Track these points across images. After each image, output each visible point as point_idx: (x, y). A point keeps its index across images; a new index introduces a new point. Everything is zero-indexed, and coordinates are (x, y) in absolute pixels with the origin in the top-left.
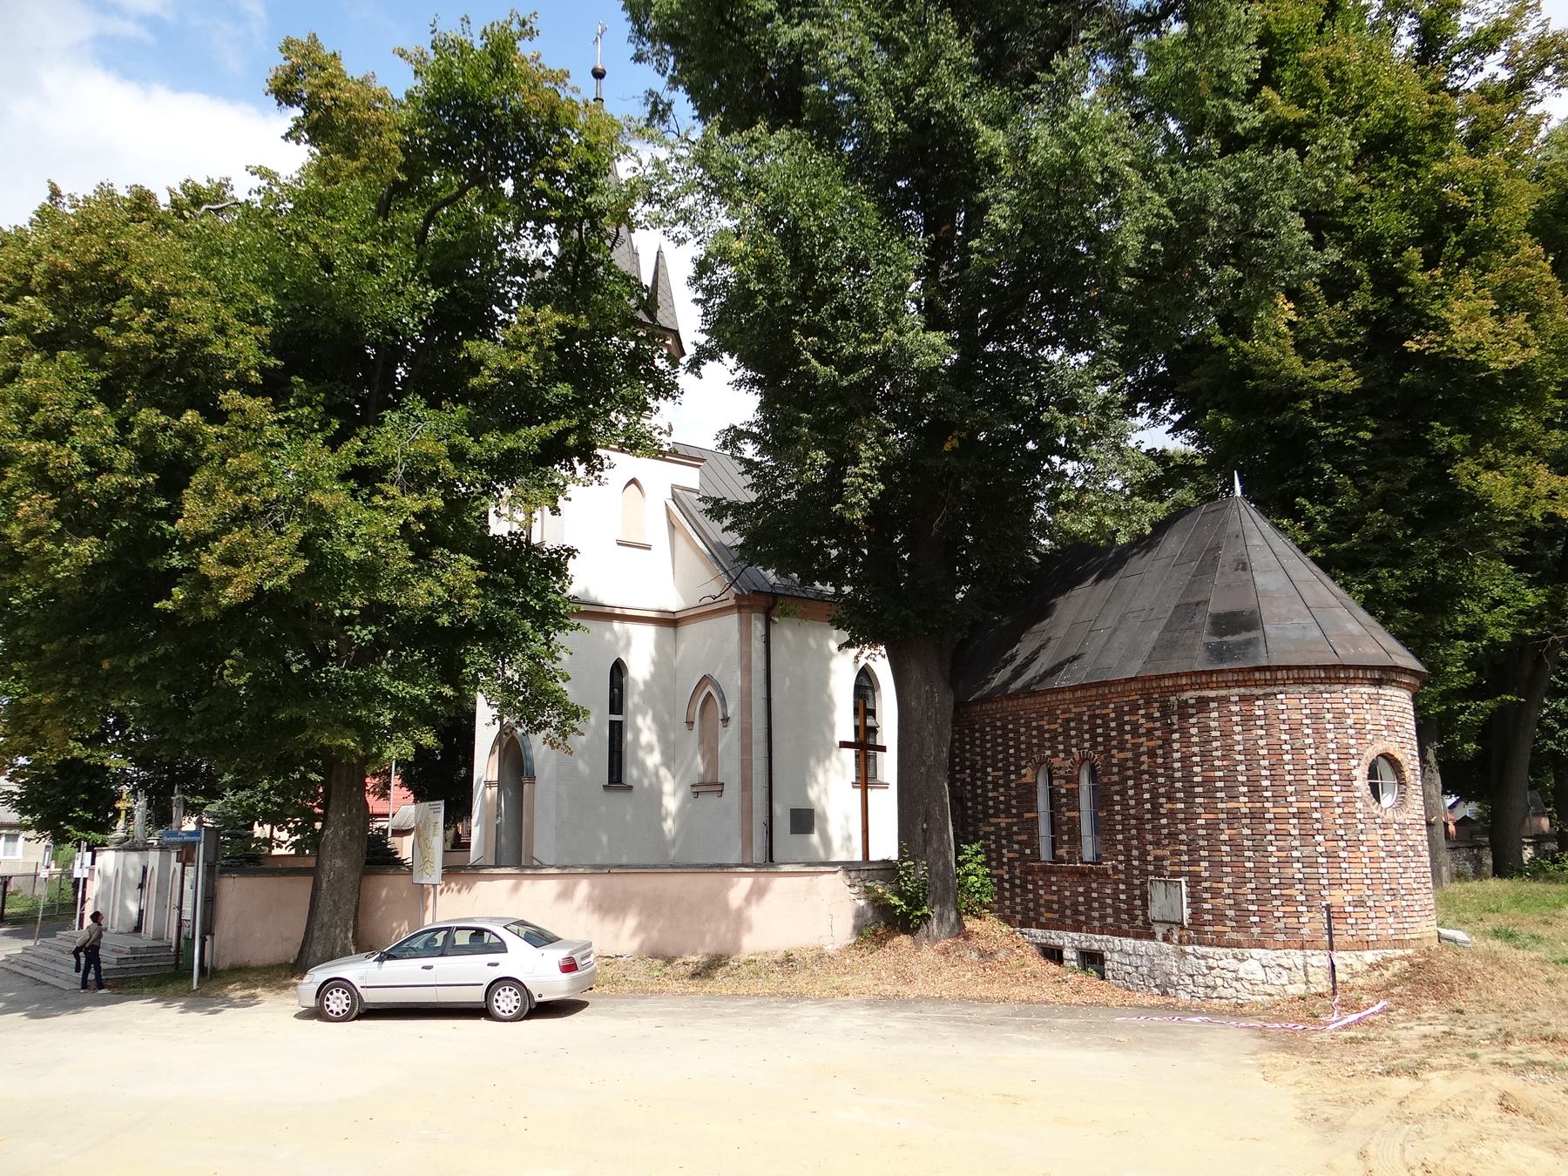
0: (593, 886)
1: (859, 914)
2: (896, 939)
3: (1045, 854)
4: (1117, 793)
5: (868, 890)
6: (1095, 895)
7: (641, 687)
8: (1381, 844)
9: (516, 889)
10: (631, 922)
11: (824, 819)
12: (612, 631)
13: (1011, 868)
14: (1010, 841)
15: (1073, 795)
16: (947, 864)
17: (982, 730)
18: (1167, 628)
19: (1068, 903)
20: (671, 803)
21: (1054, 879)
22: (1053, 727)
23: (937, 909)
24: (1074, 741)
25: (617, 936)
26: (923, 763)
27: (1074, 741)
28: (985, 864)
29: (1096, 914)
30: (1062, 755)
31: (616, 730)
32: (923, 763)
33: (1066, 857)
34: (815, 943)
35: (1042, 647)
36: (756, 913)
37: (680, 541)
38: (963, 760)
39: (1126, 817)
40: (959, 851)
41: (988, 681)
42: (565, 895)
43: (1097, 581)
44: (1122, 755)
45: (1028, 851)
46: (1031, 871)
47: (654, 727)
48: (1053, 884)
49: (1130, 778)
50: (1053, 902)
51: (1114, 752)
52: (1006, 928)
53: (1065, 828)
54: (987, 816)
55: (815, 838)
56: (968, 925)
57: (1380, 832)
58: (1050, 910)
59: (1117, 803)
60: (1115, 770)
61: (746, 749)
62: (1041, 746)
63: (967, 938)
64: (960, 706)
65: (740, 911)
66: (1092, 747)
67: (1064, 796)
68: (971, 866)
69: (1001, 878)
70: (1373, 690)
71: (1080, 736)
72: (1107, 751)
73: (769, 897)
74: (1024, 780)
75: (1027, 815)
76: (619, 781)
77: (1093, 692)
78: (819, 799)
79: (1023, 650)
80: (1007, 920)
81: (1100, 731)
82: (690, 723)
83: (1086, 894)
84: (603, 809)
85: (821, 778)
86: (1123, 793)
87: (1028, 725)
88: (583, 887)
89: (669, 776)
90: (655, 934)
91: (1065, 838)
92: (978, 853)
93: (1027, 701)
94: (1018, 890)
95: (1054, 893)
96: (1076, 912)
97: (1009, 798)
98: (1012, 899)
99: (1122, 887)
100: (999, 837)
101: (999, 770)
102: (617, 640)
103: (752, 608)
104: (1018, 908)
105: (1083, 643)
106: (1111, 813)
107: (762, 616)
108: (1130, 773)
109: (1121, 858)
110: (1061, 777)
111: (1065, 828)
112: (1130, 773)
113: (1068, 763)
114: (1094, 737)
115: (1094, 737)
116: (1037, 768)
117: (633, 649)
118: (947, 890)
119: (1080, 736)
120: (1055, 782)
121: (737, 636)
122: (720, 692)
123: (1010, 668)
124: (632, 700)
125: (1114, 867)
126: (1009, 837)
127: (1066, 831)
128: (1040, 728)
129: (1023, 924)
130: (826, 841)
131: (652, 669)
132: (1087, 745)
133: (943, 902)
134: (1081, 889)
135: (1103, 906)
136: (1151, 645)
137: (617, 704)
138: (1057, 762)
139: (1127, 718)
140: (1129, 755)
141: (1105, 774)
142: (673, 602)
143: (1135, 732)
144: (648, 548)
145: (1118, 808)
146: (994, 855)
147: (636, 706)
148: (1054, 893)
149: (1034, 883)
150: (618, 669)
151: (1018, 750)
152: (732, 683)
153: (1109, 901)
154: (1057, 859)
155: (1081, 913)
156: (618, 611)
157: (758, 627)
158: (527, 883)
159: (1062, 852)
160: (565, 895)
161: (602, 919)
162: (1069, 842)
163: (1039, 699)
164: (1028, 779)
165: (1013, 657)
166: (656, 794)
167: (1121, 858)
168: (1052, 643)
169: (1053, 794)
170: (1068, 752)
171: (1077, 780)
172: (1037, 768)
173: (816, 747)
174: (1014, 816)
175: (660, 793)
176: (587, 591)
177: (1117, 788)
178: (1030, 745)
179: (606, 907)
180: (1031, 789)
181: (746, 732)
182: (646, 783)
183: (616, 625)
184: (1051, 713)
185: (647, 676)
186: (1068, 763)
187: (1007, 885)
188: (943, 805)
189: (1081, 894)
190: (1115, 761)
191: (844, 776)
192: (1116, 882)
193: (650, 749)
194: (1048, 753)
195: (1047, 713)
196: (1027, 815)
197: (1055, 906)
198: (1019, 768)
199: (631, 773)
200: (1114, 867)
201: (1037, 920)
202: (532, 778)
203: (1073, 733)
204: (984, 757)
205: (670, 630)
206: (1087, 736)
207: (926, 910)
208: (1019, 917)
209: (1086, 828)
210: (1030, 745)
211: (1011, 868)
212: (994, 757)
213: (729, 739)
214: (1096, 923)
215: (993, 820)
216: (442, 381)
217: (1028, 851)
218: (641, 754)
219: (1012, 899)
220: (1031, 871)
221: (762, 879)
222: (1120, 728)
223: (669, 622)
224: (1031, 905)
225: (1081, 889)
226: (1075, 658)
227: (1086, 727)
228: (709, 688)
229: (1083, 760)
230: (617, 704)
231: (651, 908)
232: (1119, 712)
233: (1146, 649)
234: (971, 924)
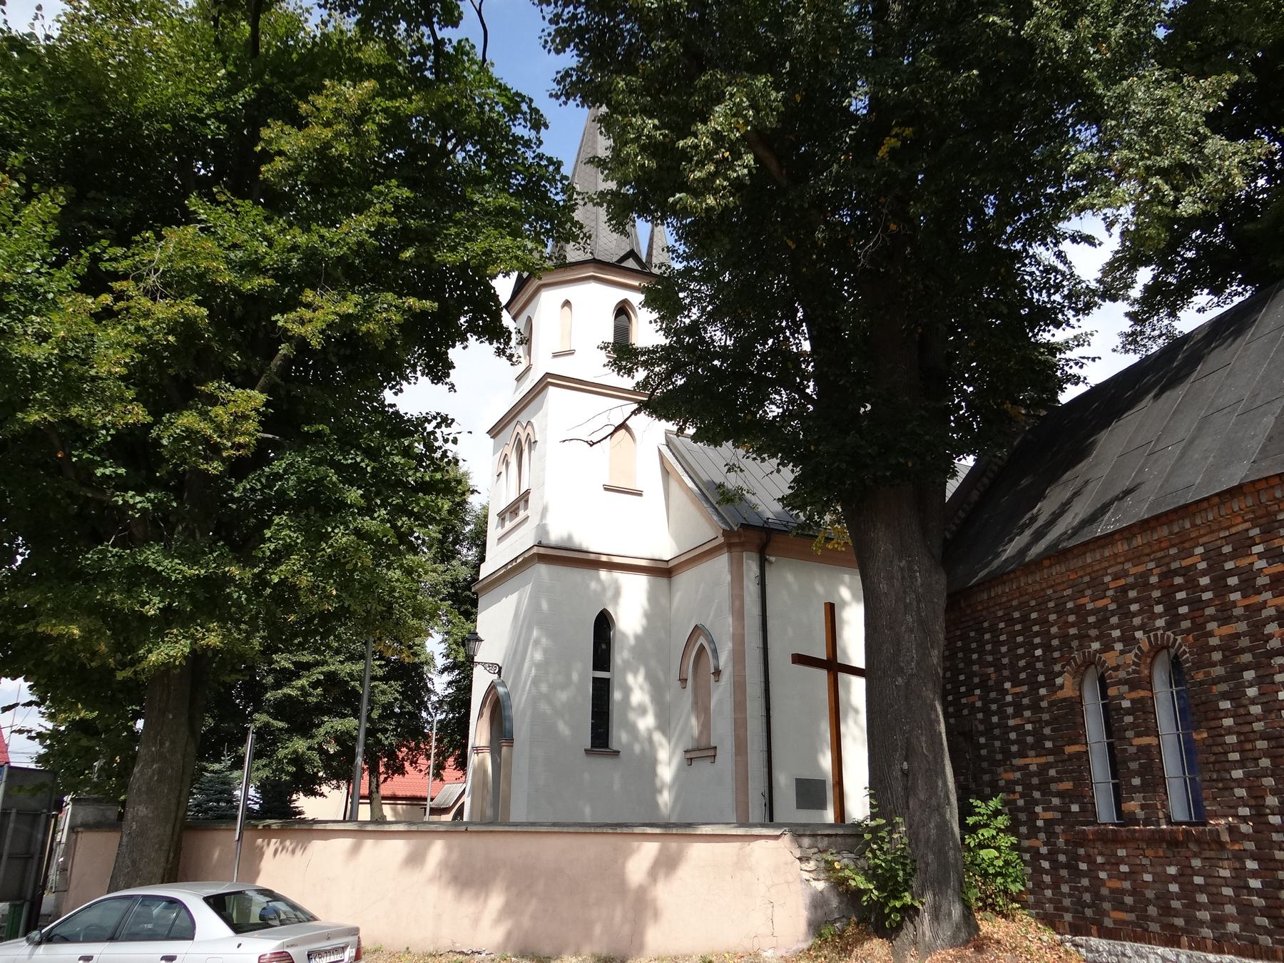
0: (450, 849)
1: (817, 903)
2: (867, 946)
3: (1105, 811)
4: (1224, 696)
5: (829, 866)
6: (1198, 880)
7: (632, 641)
9: (355, 849)
10: (496, 901)
12: (599, 580)
13: (1051, 835)
14: (1046, 792)
15: (1144, 709)
16: (944, 826)
17: (994, 630)
18: (1205, 949)
19: (1150, 894)
20: (666, 773)
21: (1122, 852)
22: (1100, 604)
23: (928, 898)
24: (1137, 621)
25: (476, 921)
26: (900, 671)
27: (1137, 621)
28: (1011, 830)
29: (1204, 915)
30: (1119, 646)
31: (602, 692)
32: (900, 671)
33: (1140, 814)
34: (748, 945)
35: (1076, 494)
36: (666, 893)
37: (674, 486)
38: (970, 676)
39: (1247, 738)
40: (965, 810)
41: (998, 555)
42: (415, 859)
43: (1156, 397)
44: (1226, 630)
45: (1075, 808)
46: (1082, 840)
47: (646, 687)
48: (1121, 861)
49: (1247, 667)
50: (1123, 892)
51: (1212, 626)
52: (1048, 936)
53: (1134, 765)
54: (1008, 755)
56: (985, 928)
58: (1120, 906)
59: (1227, 713)
60: (1217, 656)
61: (740, 705)
62: (1084, 638)
63: (979, 949)
64: (957, 600)
65: (642, 892)
66: (1169, 626)
67: (1129, 712)
68: (987, 833)
69: (1036, 855)
71: (1147, 610)
72: (1199, 628)
73: (685, 872)
74: (1060, 694)
75: (1070, 749)
76: (606, 745)
77: (1164, 531)
79: (1045, 509)
80: (1050, 921)
81: (1181, 595)
82: (683, 681)
83: (1184, 876)
84: (586, 776)
86: (1236, 695)
87: (1060, 610)
88: (437, 850)
89: (664, 741)
90: (526, 922)
91: (1136, 781)
92: (997, 813)
93: (1056, 569)
94: (1064, 873)
95: (1125, 877)
96: (1167, 911)
97: (1038, 723)
98: (1055, 886)
99: (1251, 865)
100: (1028, 788)
101: (1022, 683)
102: (604, 589)
103: (743, 546)
104: (1067, 902)
105: (1141, 471)
106: (1217, 734)
107: (755, 556)
108: (1247, 658)
109: (1244, 811)
110: (1121, 682)
111: (1134, 765)
112: (1247, 658)
113: (1131, 657)
114: (1171, 607)
115: (1171, 607)
116: (1079, 675)
117: (623, 601)
118: (944, 866)
119: (1147, 610)
120: (1112, 692)
121: (729, 578)
122: (712, 642)
123: (1028, 533)
124: (620, 656)
125: (1232, 829)
126: (1044, 786)
127: (1131, 769)
128: (1080, 611)
129: (1076, 930)
131: (644, 622)
132: (1160, 623)
133: (939, 885)
134: (1172, 870)
135: (1216, 901)
136: (1262, 438)
137: (602, 658)
138: (1111, 659)
139: (1229, 565)
140: (1242, 627)
141: (1198, 666)
142: (666, 550)
143: (1248, 586)
144: (639, 494)
145: (1228, 722)
146: (1023, 817)
147: (626, 662)
148: (1125, 877)
149: (1090, 859)
150: (604, 623)
151: (1047, 648)
152: (723, 630)
153: (1227, 891)
154: (1125, 818)
155: (1176, 913)
156: (604, 558)
157: (751, 567)
158: (369, 843)
159: (1133, 806)
160: (415, 859)
161: (460, 894)
162: (1144, 788)
163: (1075, 563)
164: (1068, 692)
165: (1033, 519)
166: (650, 763)
167: (1244, 811)
168: (1089, 487)
169: (1110, 712)
170: (1128, 640)
171: (1149, 684)
172: (1079, 675)
174: (1050, 752)
175: (654, 762)
176: (570, 538)
177: (1223, 687)
178: (1065, 639)
179: (466, 879)
180: (1074, 707)
181: (739, 687)
182: (637, 748)
183: (603, 574)
184: (1098, 587)
185: (639, 630)
186: (1131, 657)
187: (1046, 865)
188: (936, 736)
189: (1174, 879)
190: (1214, 641)
192: (1239, 857)
193: (642, 711)
194: (1096, 646)
195: (1089, 585)
196: (1070, 749)
197: (1129, 900)
198: (1051, 677)
199: (619, 737)
200: (1232, 829)
201: (1099, 924)
202: (511, 741)
203: (1134, 607)
204: (999, 667)
205: (663, 581)
206: (1159, 609)
207: (908, 898)
208: (1068, 917)
209: (1171, 763)
210: (1065, 639)
211: (1051, 835)
212: (1013, 665)
213: (721, 694)
214: (1207, 932)
215: (1018, 762)
216: (240, 171)
217: (1075, 808)
218: (632, 716)
219: (1055, 886)
220: (1082, 840)
221: (673, 845)
222: (1219, 586)
223: (661, 571)
224: (1087, 897)
225: (1172, 870)
226: (1127, 493)
227: (1156, 594)
228: (702, 640)
229: (1157, 649)
230: (602, 658)
231: (522, 884)
232: (1216, 559)
233: (1255, 446)
234: (989, 926)
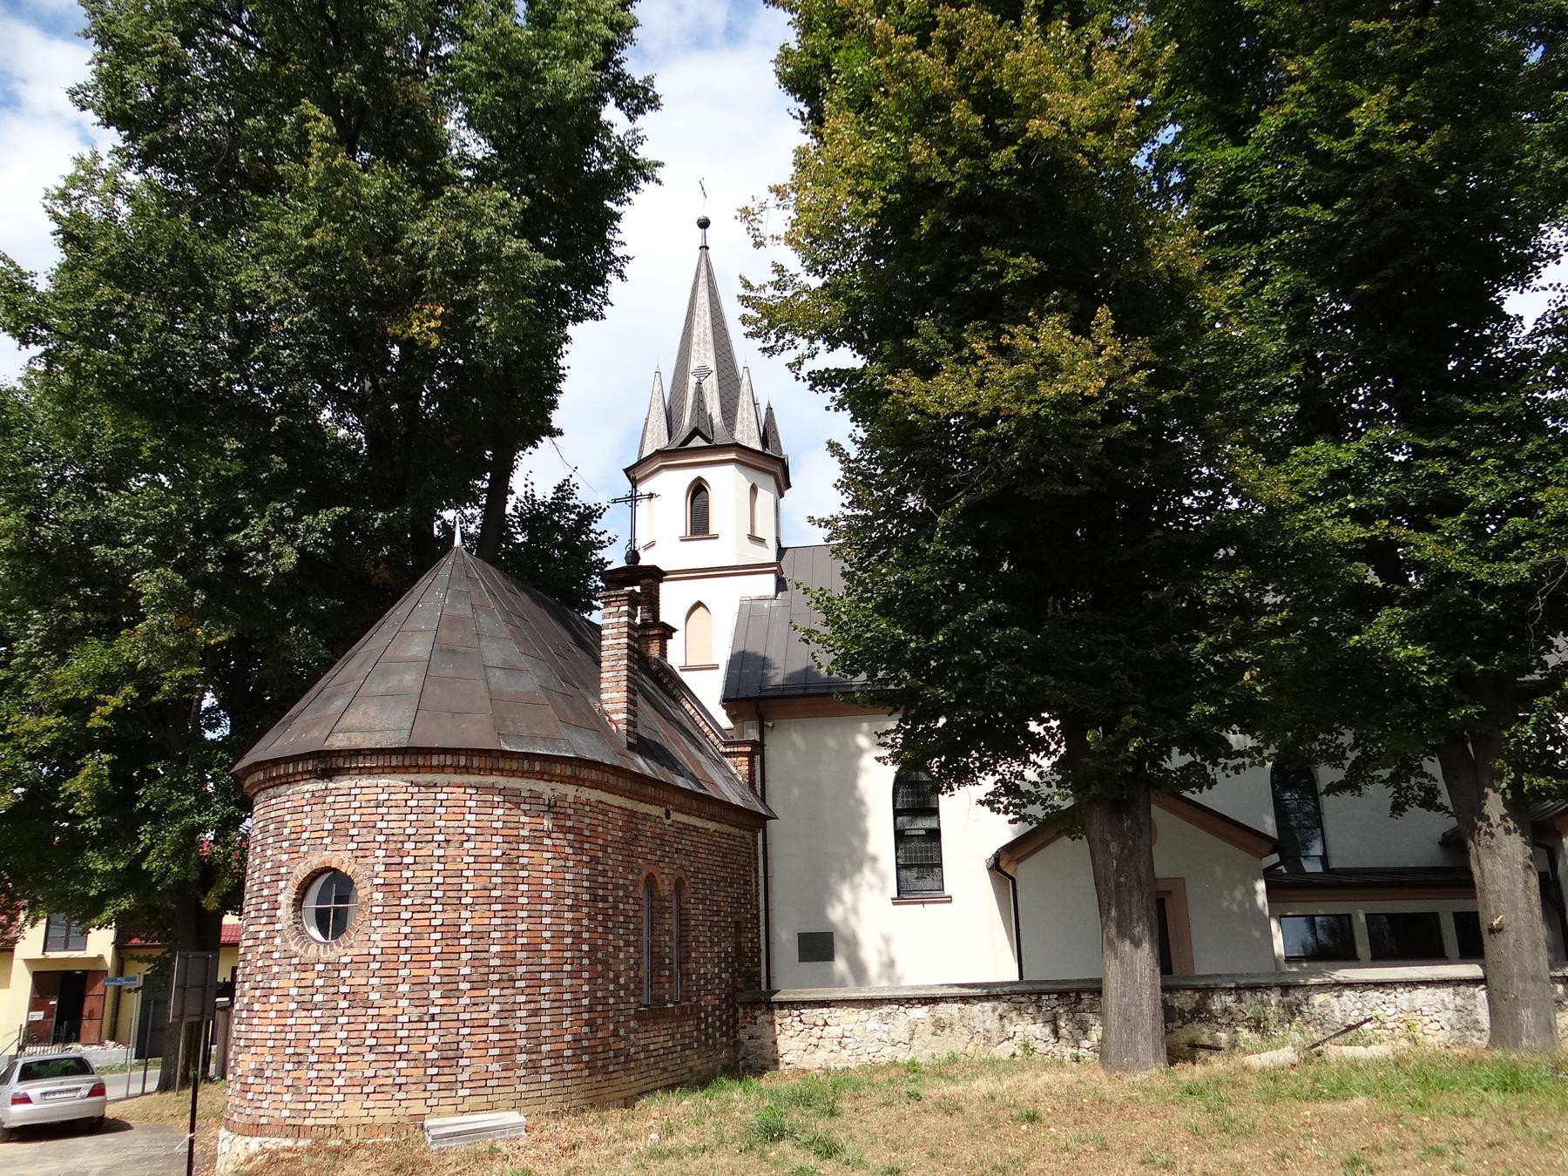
8: (294, 991)
11: (853, 944)
55: (840, 965)
57: (295, 975)
70: (321, 785)
78: (846, 920)
85: (847, 894)
107: (756, 723)
130: (858, 970)
173: (854, 860)
191: (883, 890)
